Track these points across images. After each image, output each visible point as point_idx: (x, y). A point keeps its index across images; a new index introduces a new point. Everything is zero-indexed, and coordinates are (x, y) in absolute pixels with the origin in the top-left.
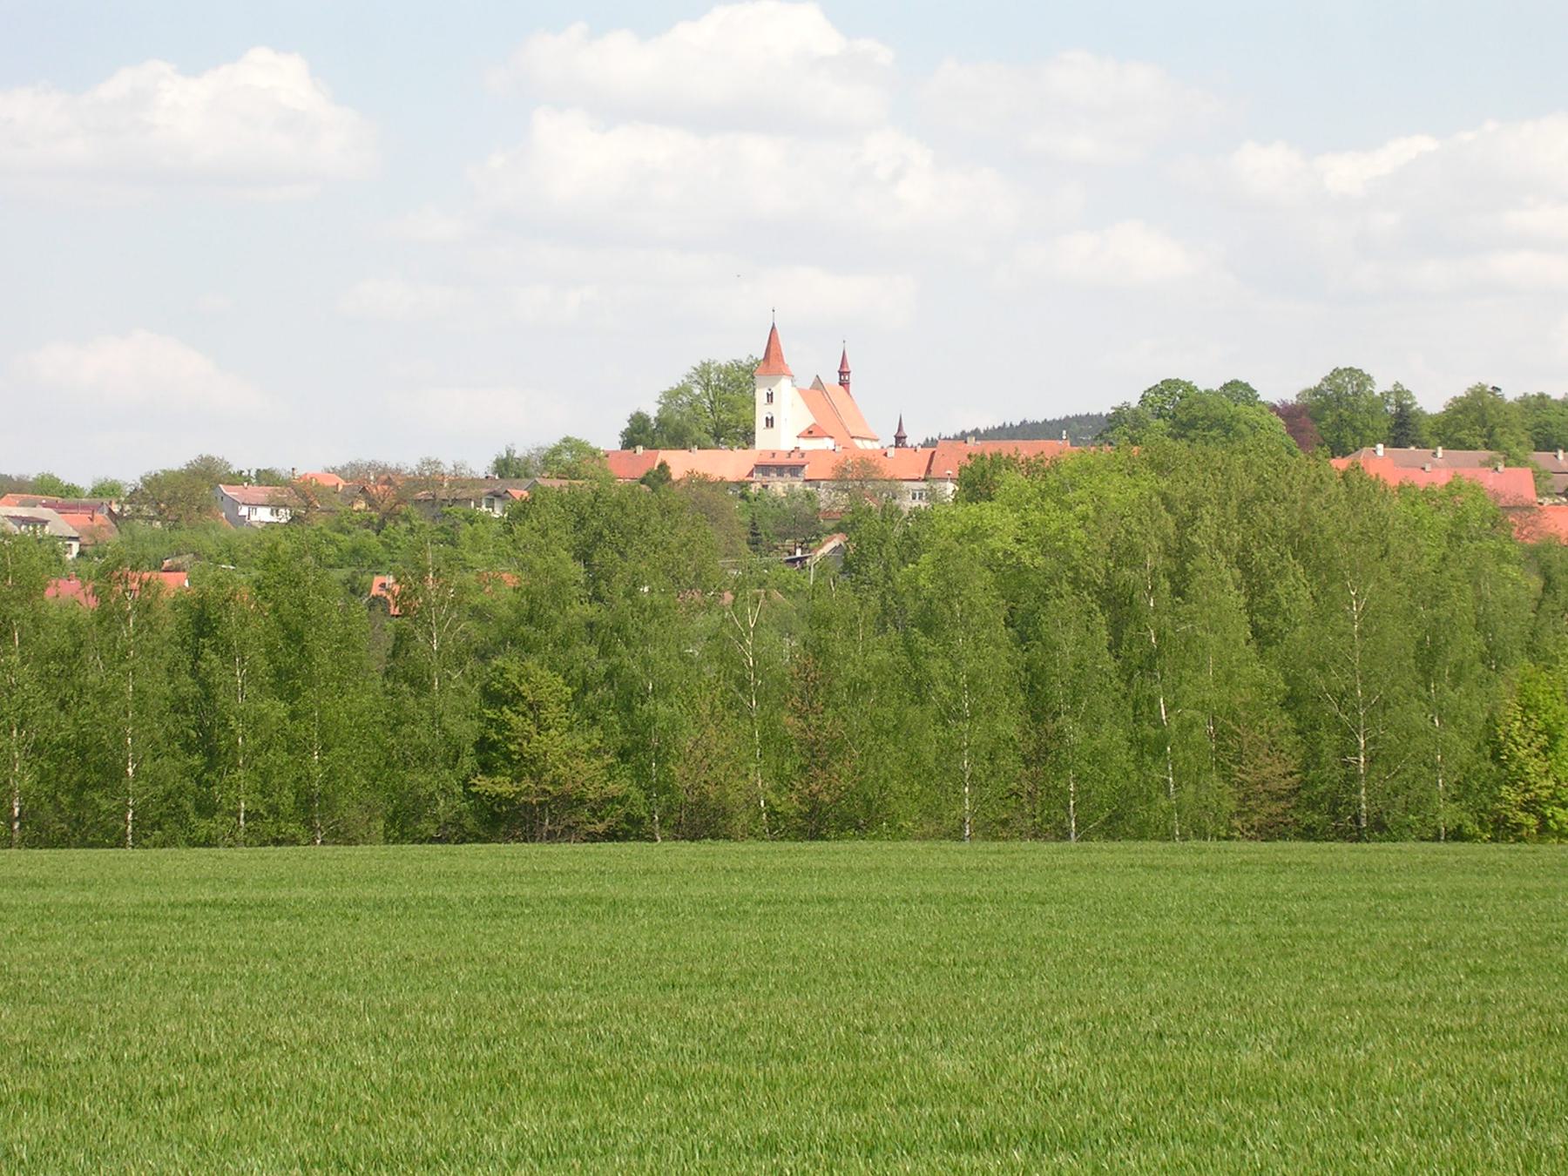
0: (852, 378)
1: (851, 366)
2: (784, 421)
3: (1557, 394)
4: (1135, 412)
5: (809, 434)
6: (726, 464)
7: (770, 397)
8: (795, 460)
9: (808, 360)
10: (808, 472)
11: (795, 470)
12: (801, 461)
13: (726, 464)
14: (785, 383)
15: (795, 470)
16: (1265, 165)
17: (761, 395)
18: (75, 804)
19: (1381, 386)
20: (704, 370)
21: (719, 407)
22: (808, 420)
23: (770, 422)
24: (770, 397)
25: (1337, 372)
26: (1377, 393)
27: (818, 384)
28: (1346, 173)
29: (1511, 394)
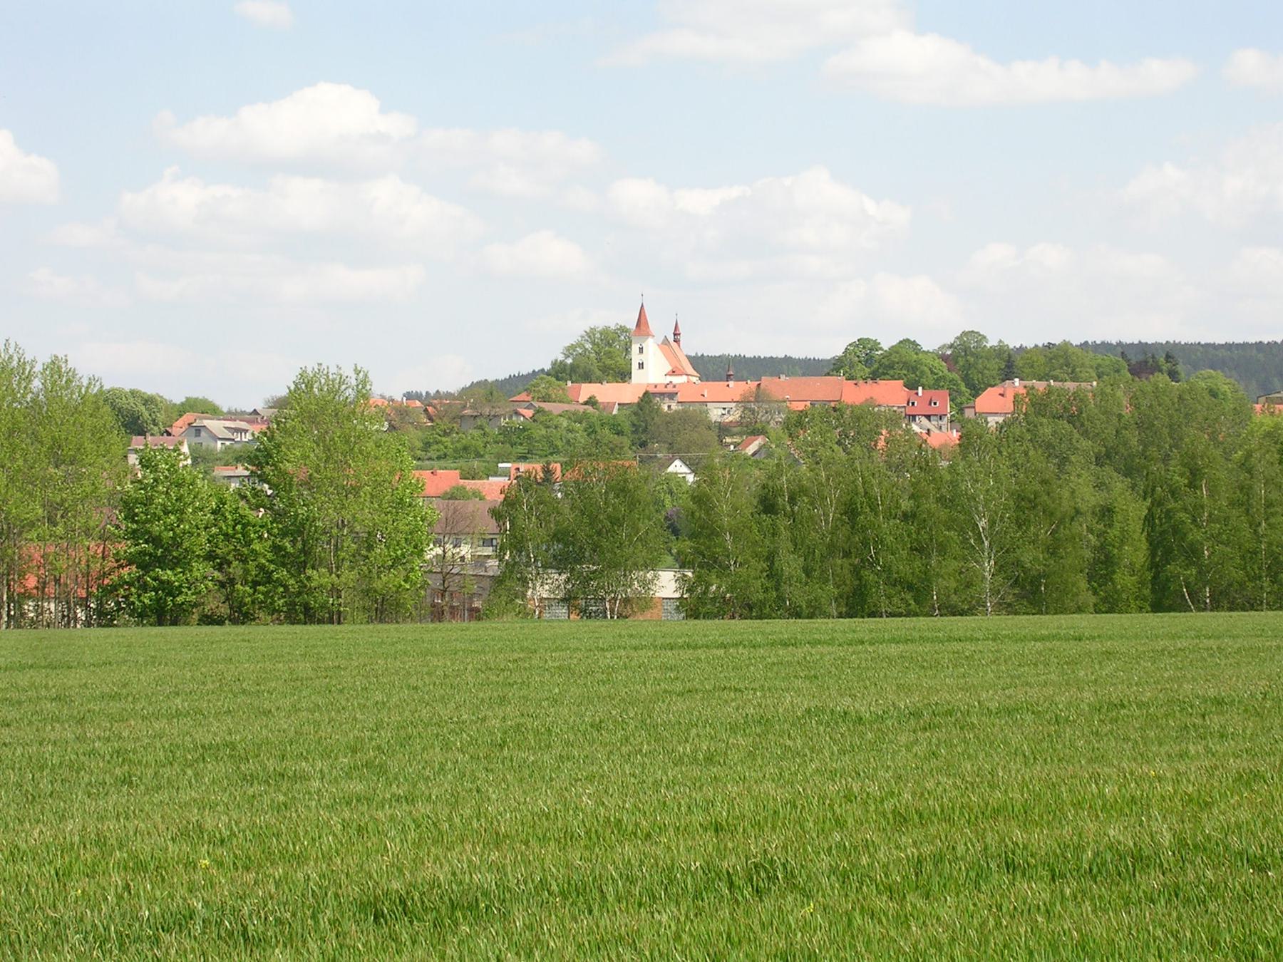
0: (682, 338)
1: (681, 330)
2: (652, 369)
3: (1279, 341)
4: (561, 362)
5: (673, 373)
6: (612, 394)
7: (641, 350)
8: (670, 389)
9: (660, 326)
10: (679, 398)
11: (672, 396)
12: (675, 390)
13: (612, 394)
14: (650, 340)
15: (672, 396)
16: (637, 194)
17: (635, 348)
18: (152, 579)
19: (992, 342)
20: (590, 334)
21: (605, 356)
22: (669, 368)
23: (641, 366)
24: (641, 350)
25: (965, 334)
26: (988, 346)
27: (666, 341)
28: (699, 201)
29: (1076, 342)
